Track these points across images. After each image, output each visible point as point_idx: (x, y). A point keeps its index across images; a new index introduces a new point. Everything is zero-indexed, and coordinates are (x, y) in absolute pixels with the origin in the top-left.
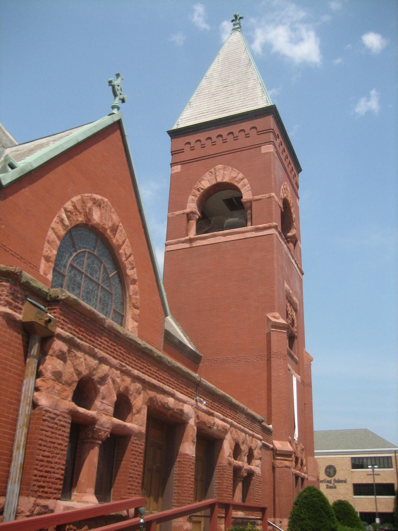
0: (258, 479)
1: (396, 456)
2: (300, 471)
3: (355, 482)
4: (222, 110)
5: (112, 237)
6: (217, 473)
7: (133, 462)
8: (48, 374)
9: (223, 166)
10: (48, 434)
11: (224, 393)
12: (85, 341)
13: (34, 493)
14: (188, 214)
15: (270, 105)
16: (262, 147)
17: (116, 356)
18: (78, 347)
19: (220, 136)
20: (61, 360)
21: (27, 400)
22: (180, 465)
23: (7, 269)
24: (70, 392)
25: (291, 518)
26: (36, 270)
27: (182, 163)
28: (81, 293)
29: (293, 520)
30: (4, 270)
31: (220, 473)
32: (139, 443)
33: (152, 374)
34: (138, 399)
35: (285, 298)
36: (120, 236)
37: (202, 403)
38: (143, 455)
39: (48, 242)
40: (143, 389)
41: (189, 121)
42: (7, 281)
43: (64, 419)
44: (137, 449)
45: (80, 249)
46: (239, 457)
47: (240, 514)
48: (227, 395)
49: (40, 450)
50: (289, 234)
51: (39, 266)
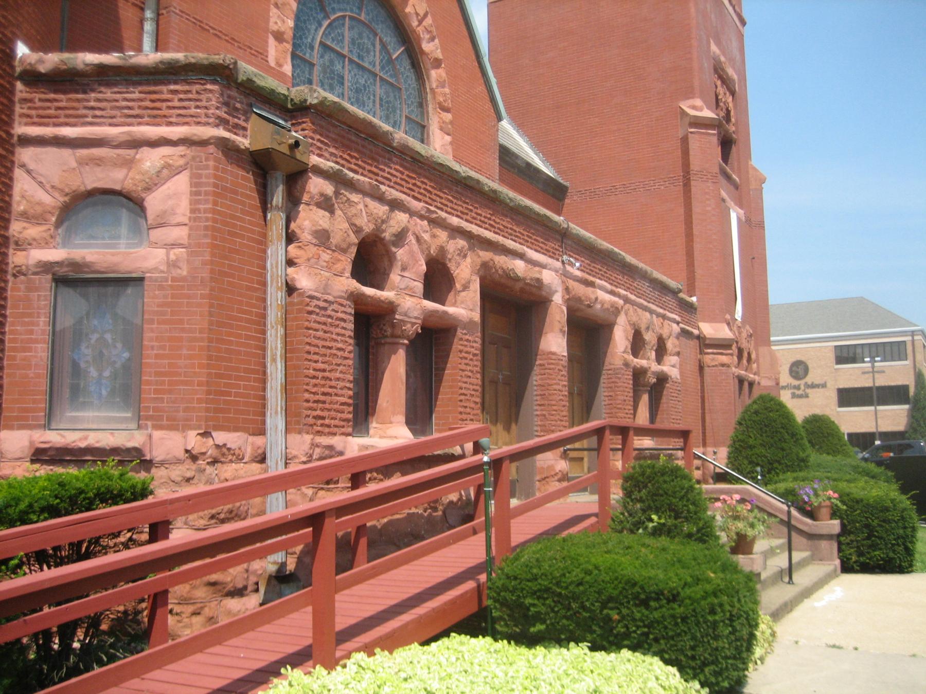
0: (674, 388)
1: (913, 341)
2: (746, 370)
3: (841, 387)
6: (605, 381)
7: (463, 370)
10: (320, 334)
11: (611, 247)
12: (362, 174)
13: (309, 428)
17: (420, 196)
18: (351, 186)
22: (542, 372)
24: (346, 263)
25: (732, 447)
26: (262, 59)
28: (346, 93)
29: (736, 448)
30: (206, 62)
31: (611, 380)
32: (470, 338)
33: (483, 222)
34: (462, 266)
35: (712, 71)
37: (572, 265)
38: (479, 358)
40: (470, 249)
42: (214, 82)
43: (343, 309)
44: (469, 349)
45: (335, 13)
46: (642, 353)
47: (647, 442)
48: (616, 250)
49: (310, 360)
51: (267, 51)
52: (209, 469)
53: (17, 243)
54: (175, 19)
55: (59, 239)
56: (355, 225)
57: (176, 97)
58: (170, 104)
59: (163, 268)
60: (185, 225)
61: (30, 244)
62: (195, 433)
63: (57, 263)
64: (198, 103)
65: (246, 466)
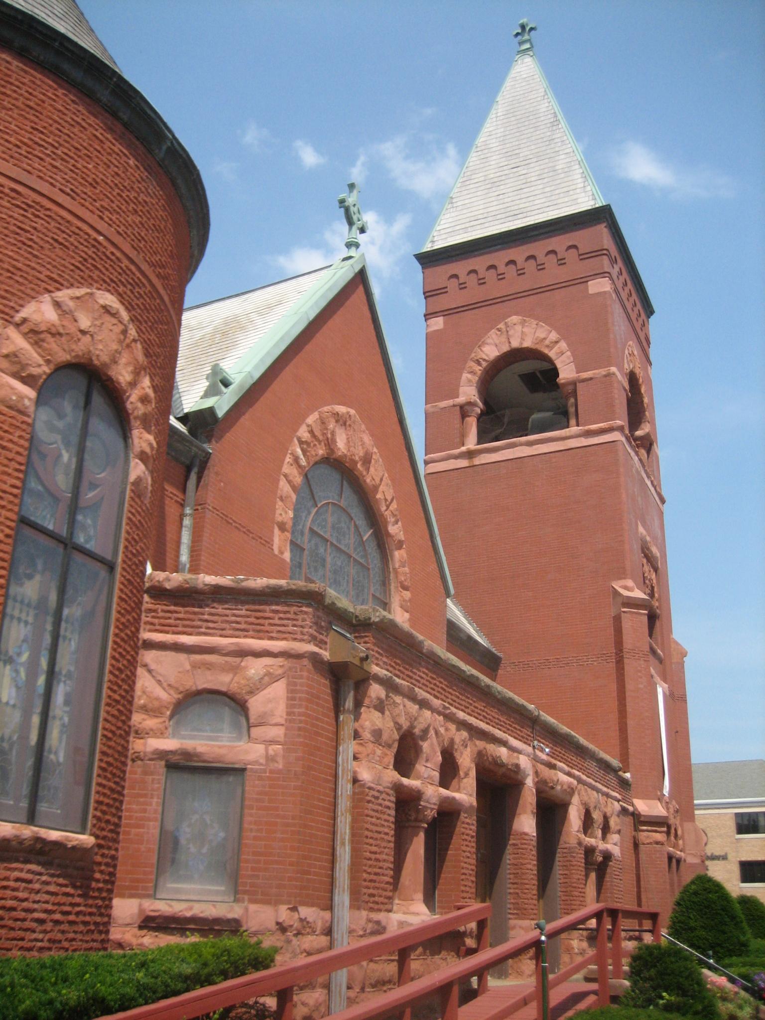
3: (743, 859)
4: (512, 213)
5: (365, 473)
6: (561, 859)
7: (464, 851)
8: (367, 735)
9: (520, 317)
10: (374, 820)
14: (462, 407)
15: (601, 205)
16: (590, 283)
17: (438, 695)
19: (512, 262)
20: (379, 711)
21: (348, 775)
22: (515, 851)
23: (309, 588)
25: (672, 928)
27: (446, 313)
29: (676, 930)
30: (304, 589)
34: (464, 756)
36: (376, 470)
37: (542, 750)
39: (281, 499)
40: (471, 739)
41: (453, 234)
42: (308, 606)
44: (468, 832)
45: (321, 502)
48: (573, 733)
50: (639, 433)
51: (273, 541)
52: (295, 941)
53: (137, 732)
54: (209, 515)
55: (170, 730)
56: (398, 724)
57: (277, 616)
58: (271, 621)
59: (263, 761)
60: (282, 725)
61: (147, 734)
62: (286, 907)
63: (171, 751)
64: (295, 622)
65: (318, 937)
